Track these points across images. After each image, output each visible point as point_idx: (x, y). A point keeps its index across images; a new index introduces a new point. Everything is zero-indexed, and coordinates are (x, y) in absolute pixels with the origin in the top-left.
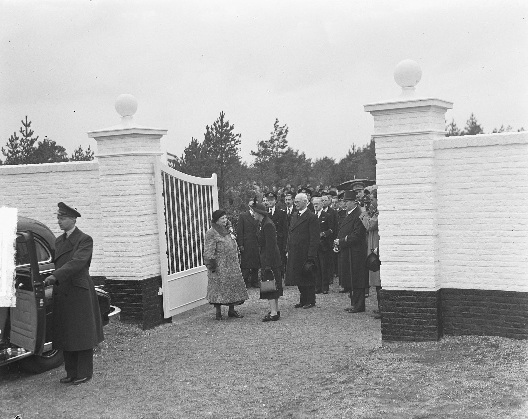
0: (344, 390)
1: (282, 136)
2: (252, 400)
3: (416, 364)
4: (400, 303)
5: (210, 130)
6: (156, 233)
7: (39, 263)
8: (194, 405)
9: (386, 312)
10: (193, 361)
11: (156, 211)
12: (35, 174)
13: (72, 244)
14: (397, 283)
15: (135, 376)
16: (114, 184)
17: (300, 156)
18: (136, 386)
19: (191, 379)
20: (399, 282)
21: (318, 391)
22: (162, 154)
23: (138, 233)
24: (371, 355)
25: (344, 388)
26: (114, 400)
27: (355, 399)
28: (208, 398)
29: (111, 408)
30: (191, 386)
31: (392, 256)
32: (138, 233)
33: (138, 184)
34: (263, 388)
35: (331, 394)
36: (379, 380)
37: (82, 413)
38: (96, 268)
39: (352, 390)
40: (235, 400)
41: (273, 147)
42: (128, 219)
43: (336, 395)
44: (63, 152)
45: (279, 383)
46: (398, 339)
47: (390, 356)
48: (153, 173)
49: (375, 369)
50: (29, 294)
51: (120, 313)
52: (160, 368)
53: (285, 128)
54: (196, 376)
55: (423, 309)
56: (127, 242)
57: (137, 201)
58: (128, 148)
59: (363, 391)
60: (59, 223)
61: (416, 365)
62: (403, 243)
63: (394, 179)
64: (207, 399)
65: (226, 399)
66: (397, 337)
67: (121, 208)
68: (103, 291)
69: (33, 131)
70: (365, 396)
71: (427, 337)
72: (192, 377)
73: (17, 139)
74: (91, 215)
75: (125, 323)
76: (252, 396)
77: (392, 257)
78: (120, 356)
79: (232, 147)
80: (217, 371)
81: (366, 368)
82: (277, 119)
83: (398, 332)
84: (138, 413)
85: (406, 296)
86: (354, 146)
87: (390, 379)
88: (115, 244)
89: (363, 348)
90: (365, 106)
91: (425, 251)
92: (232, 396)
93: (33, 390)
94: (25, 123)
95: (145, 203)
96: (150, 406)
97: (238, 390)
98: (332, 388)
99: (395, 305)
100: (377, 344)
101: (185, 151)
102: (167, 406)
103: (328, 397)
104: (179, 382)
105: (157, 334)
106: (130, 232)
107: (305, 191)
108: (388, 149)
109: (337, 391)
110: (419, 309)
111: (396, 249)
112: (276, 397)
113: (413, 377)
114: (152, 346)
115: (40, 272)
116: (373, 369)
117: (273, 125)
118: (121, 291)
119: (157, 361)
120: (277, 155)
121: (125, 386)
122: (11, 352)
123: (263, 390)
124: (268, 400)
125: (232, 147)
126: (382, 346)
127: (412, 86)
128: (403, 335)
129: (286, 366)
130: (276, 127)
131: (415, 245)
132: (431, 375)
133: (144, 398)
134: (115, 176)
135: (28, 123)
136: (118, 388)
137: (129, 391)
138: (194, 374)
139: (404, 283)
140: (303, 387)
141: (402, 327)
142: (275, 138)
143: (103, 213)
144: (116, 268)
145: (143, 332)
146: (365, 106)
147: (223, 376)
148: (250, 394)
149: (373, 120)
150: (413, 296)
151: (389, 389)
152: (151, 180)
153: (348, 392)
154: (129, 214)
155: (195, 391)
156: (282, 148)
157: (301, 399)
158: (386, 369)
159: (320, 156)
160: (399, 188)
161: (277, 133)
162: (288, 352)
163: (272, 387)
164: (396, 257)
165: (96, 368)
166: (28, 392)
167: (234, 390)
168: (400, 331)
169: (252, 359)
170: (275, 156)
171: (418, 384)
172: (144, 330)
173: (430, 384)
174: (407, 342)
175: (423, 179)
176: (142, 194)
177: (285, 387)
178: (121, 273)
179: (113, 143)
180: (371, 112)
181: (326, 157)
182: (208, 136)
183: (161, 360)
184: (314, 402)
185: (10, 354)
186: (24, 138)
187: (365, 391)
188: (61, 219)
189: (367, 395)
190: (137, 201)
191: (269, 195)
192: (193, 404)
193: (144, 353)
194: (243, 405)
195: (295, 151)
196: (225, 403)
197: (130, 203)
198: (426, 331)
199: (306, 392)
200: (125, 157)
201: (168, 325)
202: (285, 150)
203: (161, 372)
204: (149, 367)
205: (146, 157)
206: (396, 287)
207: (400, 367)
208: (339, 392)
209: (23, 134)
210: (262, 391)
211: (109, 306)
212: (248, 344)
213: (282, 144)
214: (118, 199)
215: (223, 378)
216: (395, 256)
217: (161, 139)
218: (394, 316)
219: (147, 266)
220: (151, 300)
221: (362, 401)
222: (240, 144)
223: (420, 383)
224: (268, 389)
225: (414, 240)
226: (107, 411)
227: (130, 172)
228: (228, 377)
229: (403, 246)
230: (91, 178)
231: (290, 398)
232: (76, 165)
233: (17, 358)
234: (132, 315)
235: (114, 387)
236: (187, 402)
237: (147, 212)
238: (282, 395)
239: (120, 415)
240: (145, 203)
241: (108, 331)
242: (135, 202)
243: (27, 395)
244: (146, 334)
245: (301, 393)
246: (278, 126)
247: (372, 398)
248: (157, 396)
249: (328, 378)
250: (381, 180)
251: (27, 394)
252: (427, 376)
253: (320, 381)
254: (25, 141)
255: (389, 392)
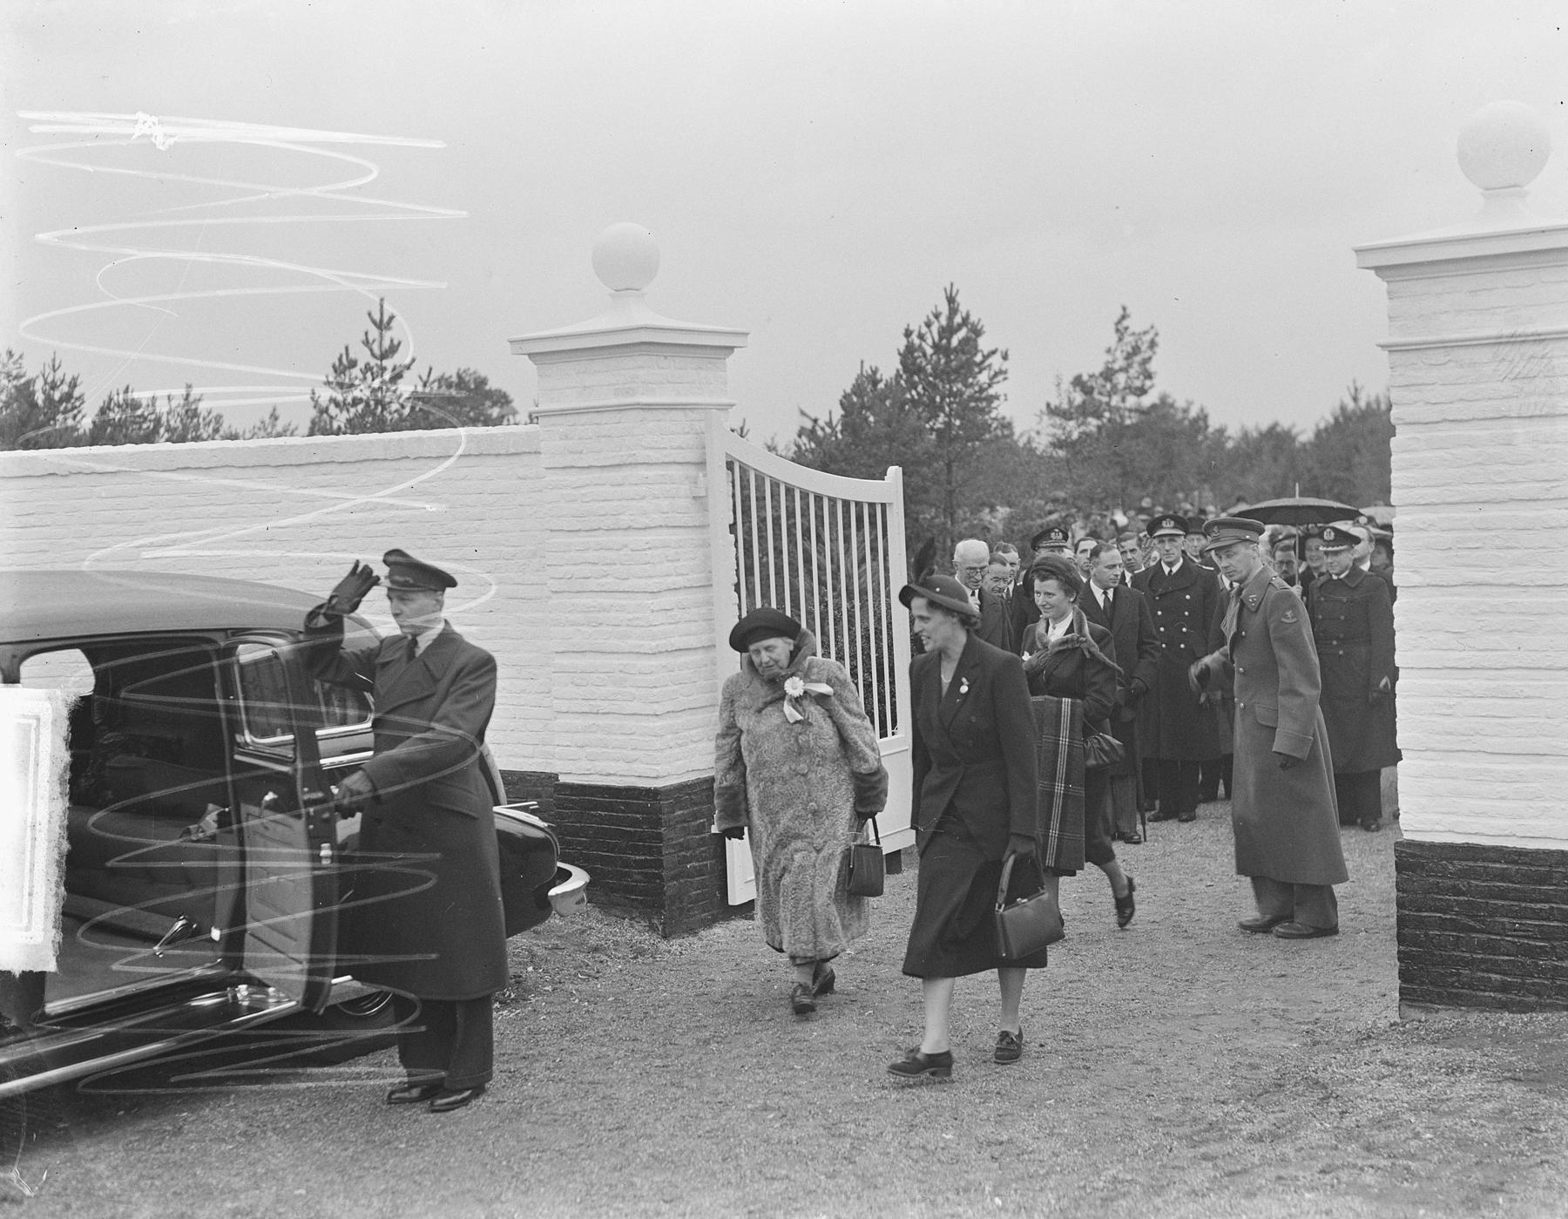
0: (1261, 1165)
1: (1138, 359)
2: (963, 1183)
3: (1507, 1087)
4: (1462, 884)
5: (917, 341)
6: (709, 646)
7: (318, 733)
8: (779, 1191)
9: (1416, 911)
10: (796, 1045)
11: (709, 579)
12: (358, 465)
13: (432, 676)
14: (1454, 818)
15: (611, 1087)
16: (584, 495)
17: (1194, 419)
18: (609, 1119)
19: (782, 1103)
20: (1460, 818)
21: (1176, 1163)
22: (732, 405)
23: (654, 644)
24: (1362, 1047)
25: (1263, 1156)
26: (536, 1162)
27: (1292, 1199)
28: (825, 1170)
29: (523, 1187)
30: (777, 1125)
31: (1438, 733)
32: (654, 644)
33: (656, 497)
34: (1001, 1143)
35: (1215, 1177)
36: (1382, 1137)
37: (434, 1199)
38: (532, 747)
39: (1286, 1167)
40: (909, 1178)
41: (1114, 390)
42: (624, 602)
43: (1232, 1178)
44: (505, 407)
45: (1056, 1131)
46: (1454, 1001)
47: (1422, 1054)
48: (702, 464)
49: (1370, 1096)
50: (289, 826)
51: (588, 887)
52: (693, 1064)
53: (1147, 338)
54: (797, 1093)
55: (1539, 906)
56: (621, 671)
57: (650, 548)
58: (627, 386)
59: (1323, 1172)
60: (396, 615)
61: (1507, 1090)
62: (1475, 692)
63: (1449, 484)
64: (821, 1173)
65: (881, 1175)
66: (1449, 994)
67: (604, 568)
68: (535, 820)
69: (399, 343)
70: (1329, 1188)
71: (1549, 997)
72: (786, 1097)
73: (353, 364)
74: (520, 587)
75: (610, 915)
76: (964, 1168)
77: (1438, 737)
78: (583, 1018)
79: (982, 390)
80: (867, 1081)
81: (1339, 1093)
82: (1124, 309)
83: (1455, 979)
84: (601, 1207)
85: (1480, 864)
86: (1356, 390)
87: (1417, 1136)
88: (586, 675)
89: (1339, 1025)
90: (1357, 251)
91: (1547, 720)
92: (901, 1165)
93: (303, 1116)
94: (378, 321)
95: (677, 553)
96: (642, 1186)
97: (924, 1148)
98: (1224, 1156)
99: (1448, 891)
100: (1384, 1014)
101: (841, 401)
102: (695, 1189)
103: (1207, 1185)
104: (743, 1110)
105: (704, 952)
106: (630, 642)
107: (1172, 522)
108: (1432, 387)
109: (1239, 1168)
110: (1523, 905)
111: (1450, 712)
112: (1039, 1175)
113: (1491, 1132)
114: (680, 990)
115: (322, 761)
116: (1361, 1097)
117: (1113, 327)
118: (602, 820)
119: (688, 1041)
120: (1122, 417)
121: (578, 1116)
122: (250, 994)
123: (1001, 1148)
124: (1014, 1185)
125: (982, 390)
126: (1399, 1021)
127: (1514, 186)
128: (1470, 988)
129: (1085, 1072)
130: (1121, 332)
131: (1513, 701)
132: (1554, 1129)
133: (627, 1159)
134: (590, 470)
135: (386, 319)
136: (555, 1121)
137: (588, 1132)
138: (791, 1089)
139: (1473, 820)
140: (1131, 1148)
141: (1467, 963)
142: (1116, 366)
143: (552, 581)
144: (588, 750)
145: (663, 945)
146: (1356, 251)
147: (881, 1098)
148: (957, 1162)
149: (1385, 296)
150: (1506, 863)
151: (1407, 1168)
152: (696, 483)
153: (1271, 1173)
154: (625, 586)
155: (790, 1143)
156: (1139, 396)
157: (1119, 1186)
158: (1406, 1099)
159: (1258, 421)
160: (1462, 515)
161: (1122, 351)
162: (1097, 1027)
163: (1031, 1142)
164: (1449, 737)
165: (504, 1055)
166: (288, 1121)
167: (912, 1144)
168: (1458, 974)
169: (981, 1046)
170: (1118, 420)
171: (1508, 1159)
172: (665, 937)
173: (1547, 1162)
174: (1482, 1012)
175: (1547, 485)
176: (667, 526)
177: (1070, 1143)
178: (602, 766)
179: (584, 372)
180: (1378, 269)
181: (1276, 425)
182: (909, 356)
183: (699, 1035)
184: (1158, 1201)
185: (246, 1003)
186: (373, 362)
187: (1329, 1173)
188: (402, 599)
189: (1332, 1186)
190: (650, 548)
191: (1053, 534)
192: (776, 1185)
193: (655, 1010)
194: (932, 1198)
195: (1180, 404)
196: (876, 1187)
197: (630, 553)
198: (1547, 979)
199: (1138, 1163)
200: (618, 415)
201: (739, 924)
202: (1147, 401)
203: (694, 1074)
204: (659, 1056)
205: (680, 413)
206: (1446, 834)
207: (1453, 1095)
208: (1244, 1171)
209: (371, 350)
210: (997, 1155)
211: (554, 864)
212: (975, 997)
213: (1138, 383)
214: (596, 539)
215: (883, 1104)
216: (1451, 734)
217: (729, 360)
218: (1442, 924)
219: (680, 746)
220: (688, 849)
221: (1314, 1208)
222: (1005, 379)
223: (1513, 1155)
224: (1018, 1147)
225: (1512, 683)
226: (510, 1195)
227: (631, 460)
228: (898, 1101)
229: (1474, 701)
230: (520, 478)
231: (1082, 1184)
232: (476, 437)
233: (265, 1015)
234: (629, 890)
235: (546, 1118)
236: (757, 1176)
237: (680, 581)
238: (1058, 1169)
239: (546, 1211)
240: (677, 553)
241: (560, 937)
242: (645, 550)
243: (286, 1131)
244: (669, 952)
245: (1120, 1167)
246: (1126, 328)
247: (1349, 1198)
248: (668, 1153)
249: (1214, 1119)
250: (1407, 487)
251: (284, 1127)
252: (1541, 1132)
253: (1187, 1130)
254: (375, 369)
255: (1407, 1180)
